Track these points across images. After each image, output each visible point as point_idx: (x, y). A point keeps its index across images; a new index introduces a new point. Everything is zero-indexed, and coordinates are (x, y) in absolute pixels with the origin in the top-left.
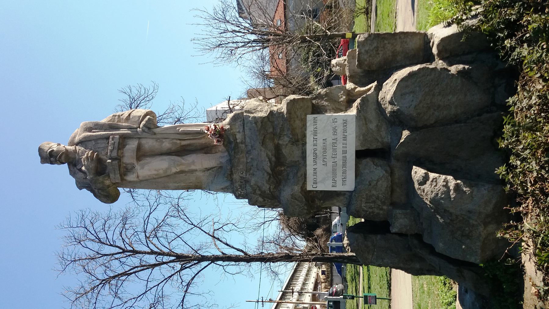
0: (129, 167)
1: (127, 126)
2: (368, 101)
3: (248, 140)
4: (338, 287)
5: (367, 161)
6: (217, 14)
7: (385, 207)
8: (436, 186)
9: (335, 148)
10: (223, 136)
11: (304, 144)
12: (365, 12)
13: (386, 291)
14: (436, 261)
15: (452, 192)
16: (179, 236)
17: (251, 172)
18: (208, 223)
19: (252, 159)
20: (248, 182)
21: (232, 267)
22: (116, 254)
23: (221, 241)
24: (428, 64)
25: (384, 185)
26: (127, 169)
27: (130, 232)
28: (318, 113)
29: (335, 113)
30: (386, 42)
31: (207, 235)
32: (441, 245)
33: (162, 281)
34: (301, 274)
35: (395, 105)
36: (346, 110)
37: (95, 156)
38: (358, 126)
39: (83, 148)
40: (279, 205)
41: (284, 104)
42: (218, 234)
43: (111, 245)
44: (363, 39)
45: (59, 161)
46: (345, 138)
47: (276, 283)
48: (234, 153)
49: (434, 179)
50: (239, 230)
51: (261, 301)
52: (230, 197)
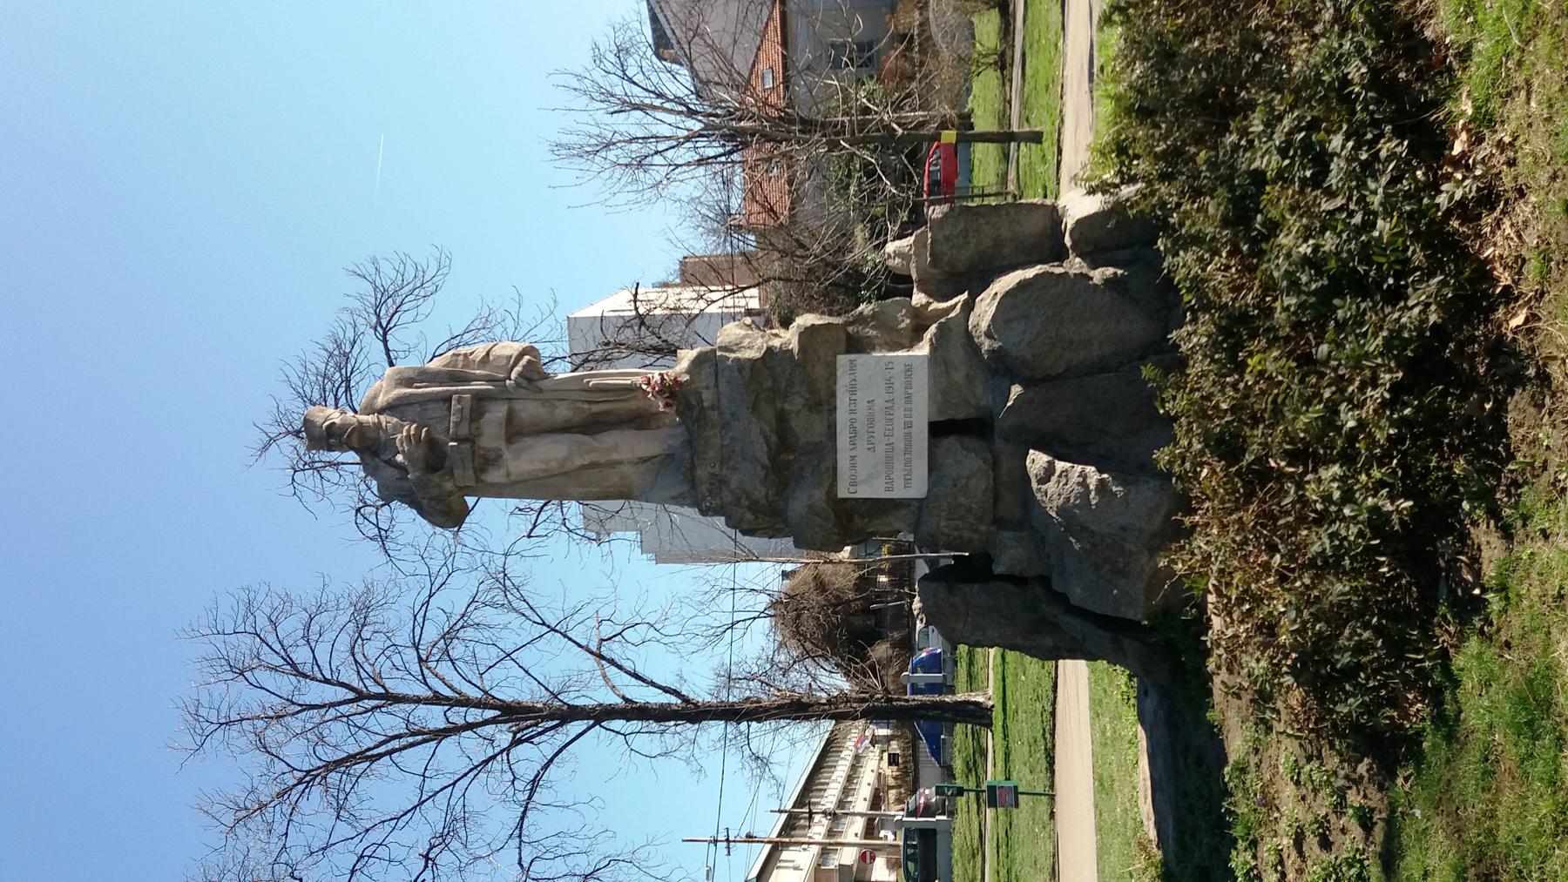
0: (492, 455)
1: (485, 376)
2: (950, 330)
3: (724, 402)
4: (927, 794)
5: (950, 442)
6: (601, 62)
7: (983, 528)
8: (1066, 484)
9: (891, 417)
10: (676, 396)
11: (833, 410)
12: (996, 63)
13: (1043, 776)
14: (1076, 626)
15: (1092, 496)
16: (509, 655)
17: (731, 463)
18: (583, 621)
19: (732, 438)
20: (725, 482)
21: (647, 737)
22: (340, 703)
23: (620, 667)
24: (1056, 264)
25: (980, 486)
26: (487, 460)
27: (372, 649)
28: (859, 351)
29: (890, 351)
30: (981, 221)
31: (583, 652)
32: (1078, 591)
33: (466, 775)
34: (834, 777)
35: (995, 340)
36: (910, 347)
37: (423, 435)
38: (933, 377)
39: (395, 420)
40: (783, 529)
41: (793, 335)
42: (613, 650)
43: (327, 681)
44: (940, 216)
45: (346, 444)
46: (908, 399)
47: (766, 787)
48: (699, 427)
49: (1063, 472)
50: (666, 640)
51: (724, 839)
52: (692, 512)
